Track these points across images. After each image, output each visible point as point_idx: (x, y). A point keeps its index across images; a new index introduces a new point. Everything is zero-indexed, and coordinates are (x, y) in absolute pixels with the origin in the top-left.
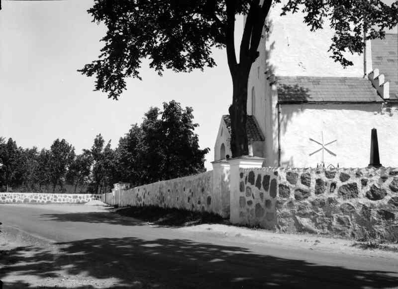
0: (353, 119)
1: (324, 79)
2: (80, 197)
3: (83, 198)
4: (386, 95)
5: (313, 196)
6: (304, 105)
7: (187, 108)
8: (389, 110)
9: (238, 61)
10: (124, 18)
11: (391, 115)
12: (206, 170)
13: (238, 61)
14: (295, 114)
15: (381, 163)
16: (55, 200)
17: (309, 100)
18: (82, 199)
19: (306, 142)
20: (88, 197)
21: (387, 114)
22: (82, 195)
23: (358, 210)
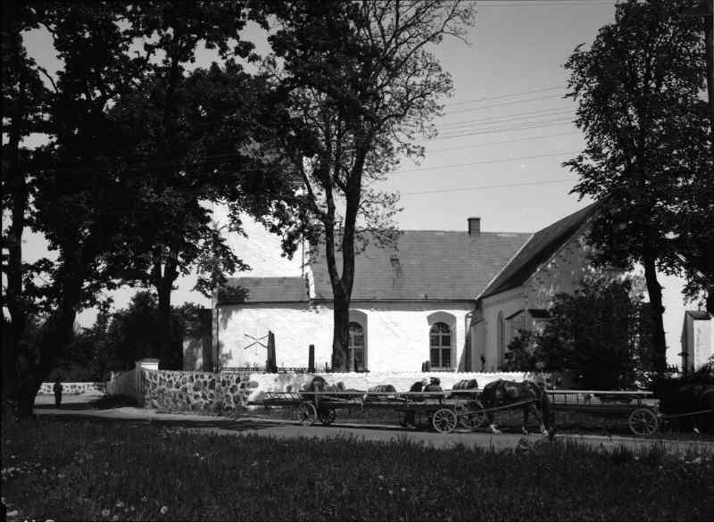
0: (284, 316)
1: (266, 279)
2: (80, 387)
3: (84, 387)
4: (313, 295)
5: (158, 387)
6: (242, 305)
7: (578, 114)
8: (315, 308)
9: (163, 275)
10: (141, 78)
11: (317, 312)
12: (429, 318)
13: (163, 275)
14: (234, 313)
15: (663, 304)
16: (48, 391)
17: (246, 300)
18: (82, 389)
19: (241, 338)
20: (88, 386)
21: (314, 311)
22: (81, 384)
23: (173, 395)
